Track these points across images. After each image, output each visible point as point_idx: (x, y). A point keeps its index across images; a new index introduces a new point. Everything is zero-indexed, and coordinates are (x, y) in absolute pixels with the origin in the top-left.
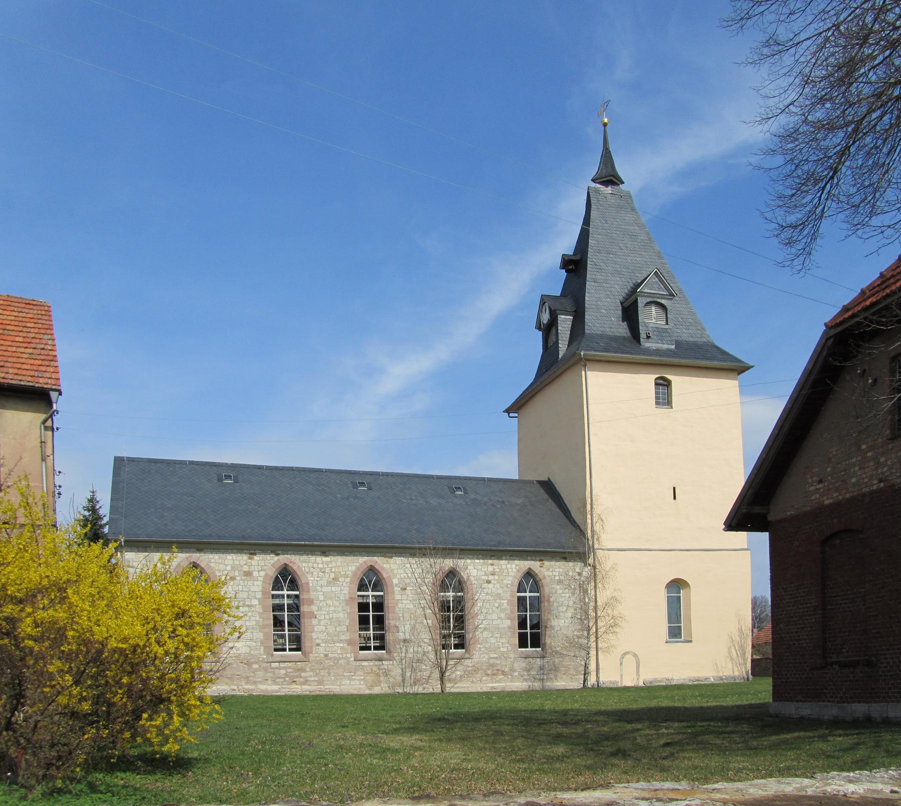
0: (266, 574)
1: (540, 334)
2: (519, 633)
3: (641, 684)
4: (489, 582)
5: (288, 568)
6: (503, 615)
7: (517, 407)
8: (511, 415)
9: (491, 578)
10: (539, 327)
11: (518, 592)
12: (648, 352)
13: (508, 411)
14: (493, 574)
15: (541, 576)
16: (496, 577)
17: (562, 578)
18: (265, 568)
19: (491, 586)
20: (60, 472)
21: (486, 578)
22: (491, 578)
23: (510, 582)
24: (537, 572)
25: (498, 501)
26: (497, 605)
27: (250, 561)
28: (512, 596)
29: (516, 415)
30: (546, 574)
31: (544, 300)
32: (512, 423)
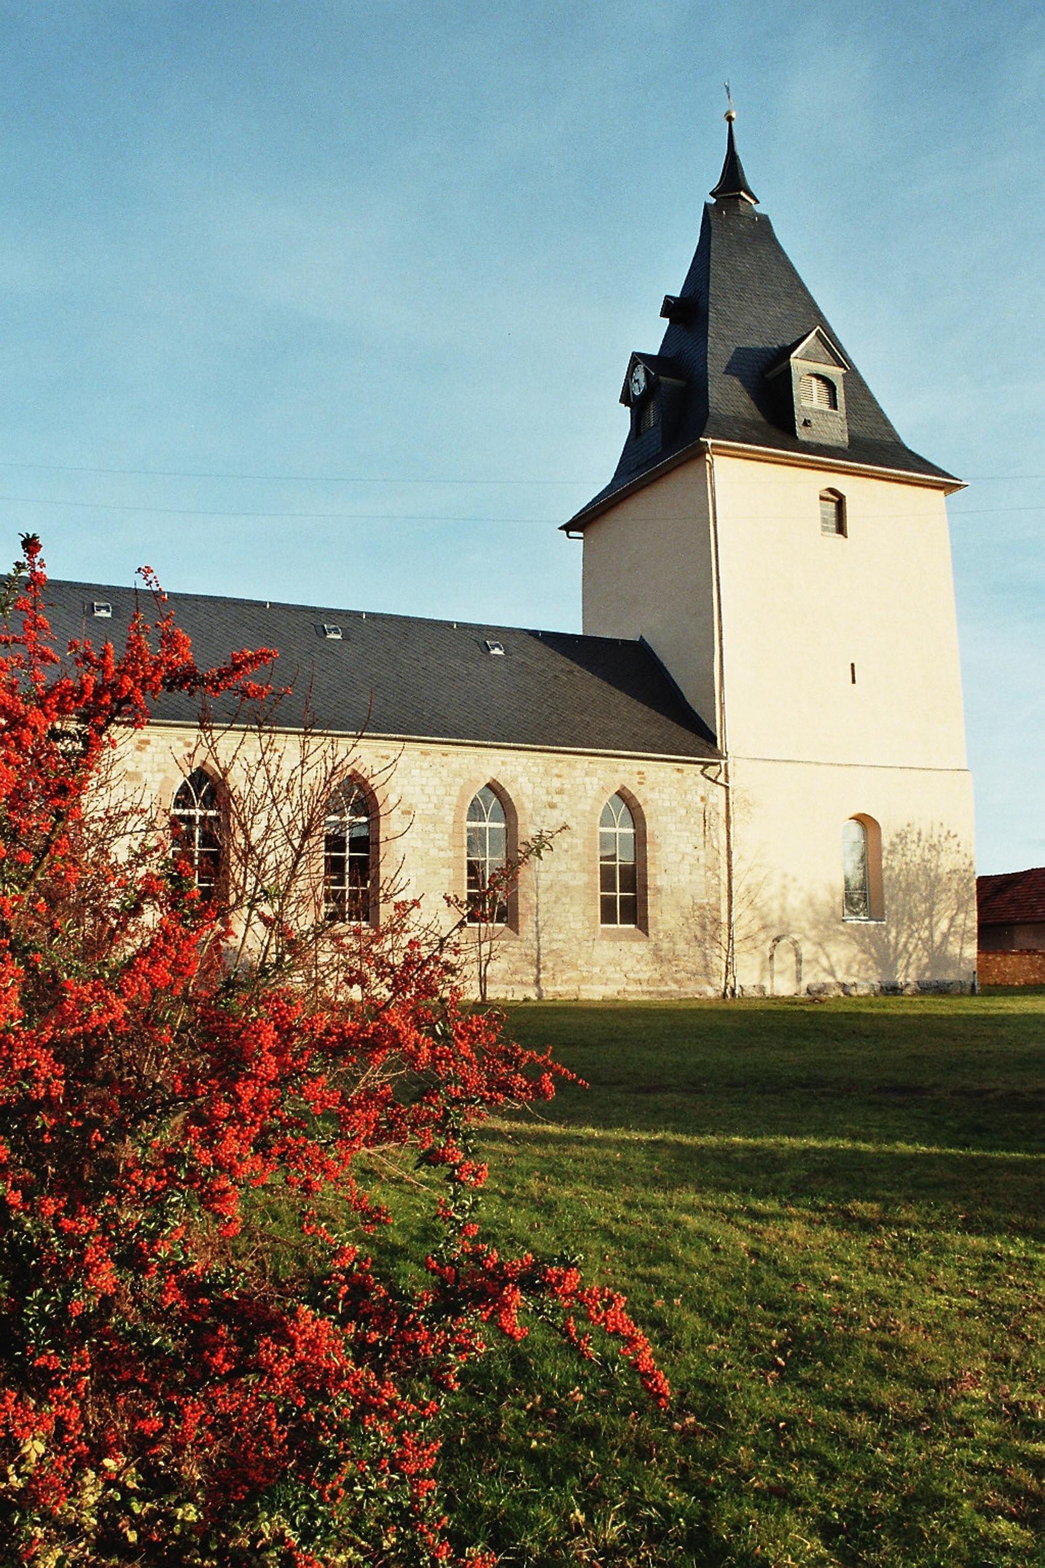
0: (166, 777)
1: (625, 414)
2: (602, 897)
3: (803, 994)
4: (552, 806)
5: (222, 790)
6: (575, 865)
7: (579, 524)
8: (571, 534)
9: (556, 799)
10: (626, 398)
11: (602, 825)
12: (806, 448)
13: (567, 528)
14: (560, 792)
15: (640, 801)
16: (566, 798)
17: (674, 804)
18: (164, 767)
19: (556, 813)
20: (909, 825)
21: (546, 798)
22: (556, 799)
23: (588, 808)
24: (633, 792)
25: (562, 670)
26: (565, 846)
27: (139, 753)
28: (592, 832)
29: (581, 535)
30: (650, 796)
31: (637, 359)
32: (575, 546)
